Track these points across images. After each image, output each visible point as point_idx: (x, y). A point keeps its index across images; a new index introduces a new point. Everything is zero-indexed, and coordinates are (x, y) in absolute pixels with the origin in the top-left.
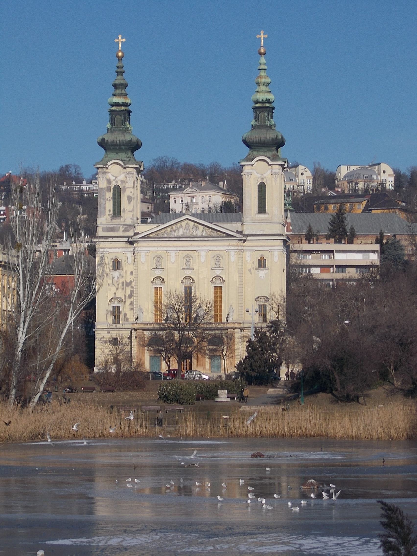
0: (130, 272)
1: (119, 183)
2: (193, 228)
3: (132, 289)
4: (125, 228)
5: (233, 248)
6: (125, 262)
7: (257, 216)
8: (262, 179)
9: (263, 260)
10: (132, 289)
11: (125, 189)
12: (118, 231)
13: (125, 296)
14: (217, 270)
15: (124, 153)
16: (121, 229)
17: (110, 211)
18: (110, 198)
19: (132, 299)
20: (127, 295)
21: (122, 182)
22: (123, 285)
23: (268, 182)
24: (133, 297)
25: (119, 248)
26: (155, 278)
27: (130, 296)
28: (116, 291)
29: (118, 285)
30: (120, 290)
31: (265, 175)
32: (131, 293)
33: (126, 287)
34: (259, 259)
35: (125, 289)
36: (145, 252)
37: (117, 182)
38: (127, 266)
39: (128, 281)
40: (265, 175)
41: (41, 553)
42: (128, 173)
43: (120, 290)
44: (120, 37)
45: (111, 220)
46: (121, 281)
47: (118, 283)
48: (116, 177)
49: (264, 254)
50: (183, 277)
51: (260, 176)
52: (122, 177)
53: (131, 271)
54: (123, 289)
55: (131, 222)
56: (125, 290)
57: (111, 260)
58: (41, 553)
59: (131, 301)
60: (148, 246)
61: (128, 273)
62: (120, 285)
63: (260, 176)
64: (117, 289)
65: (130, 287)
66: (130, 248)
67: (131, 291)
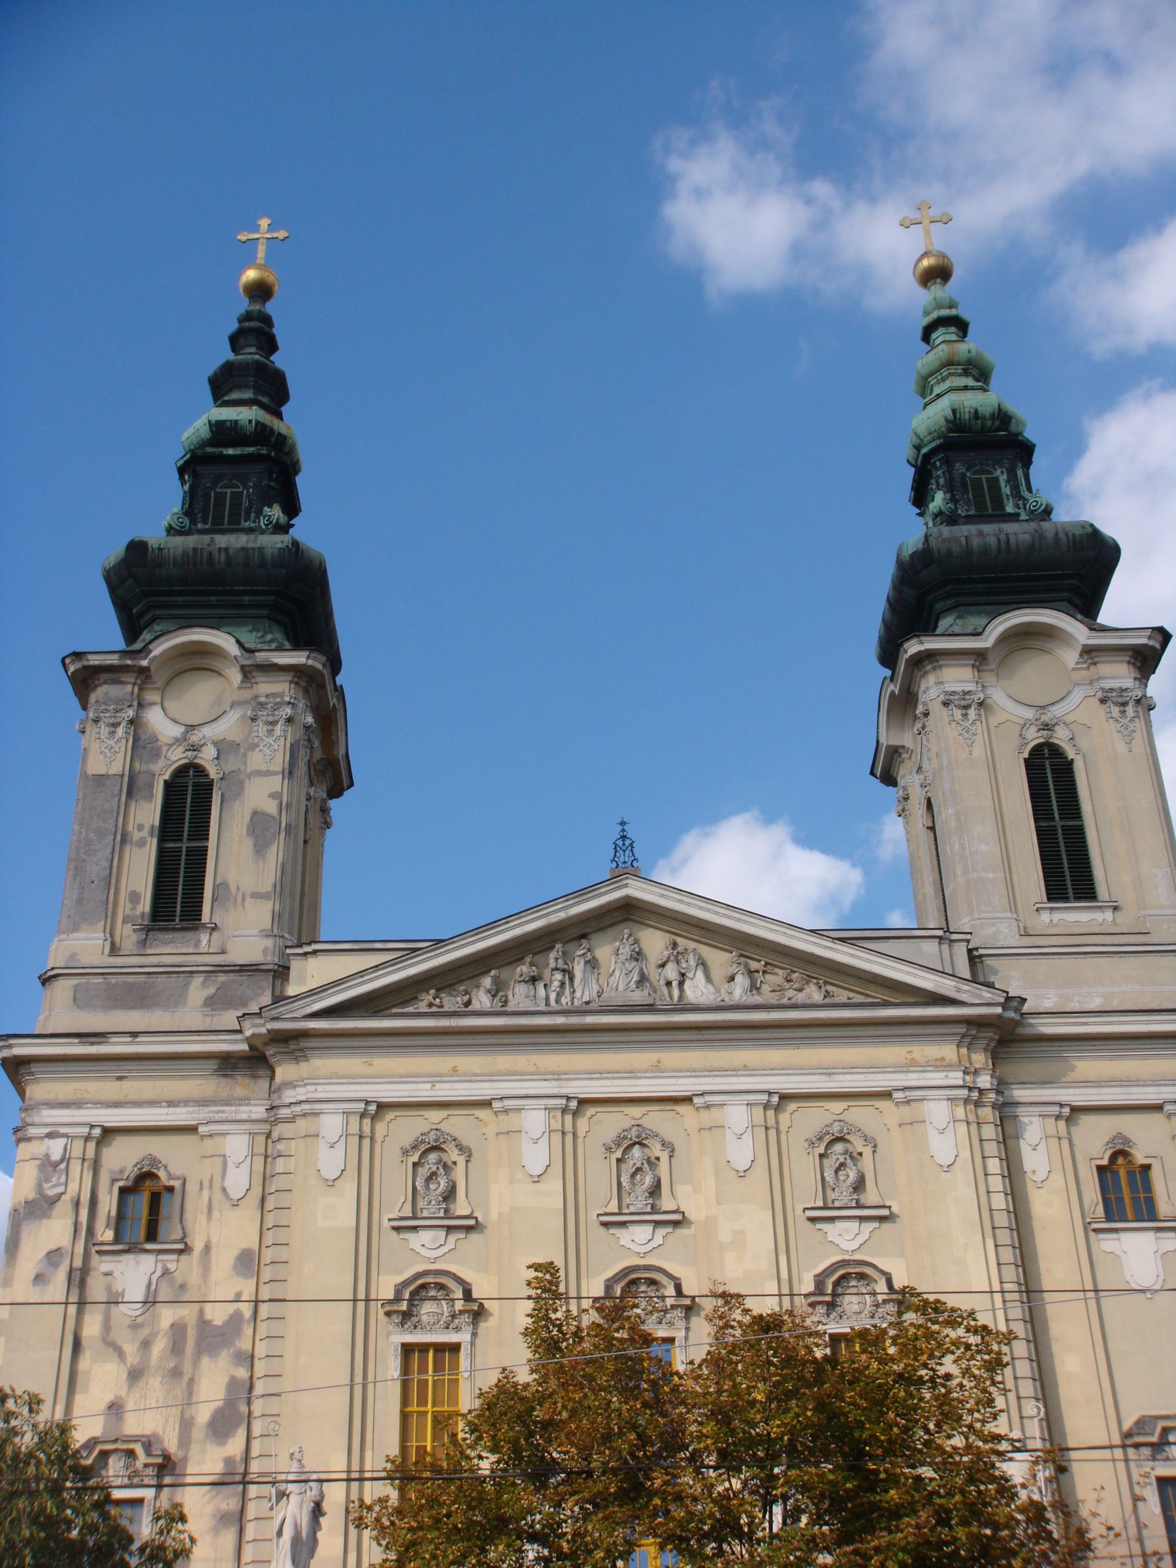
0: (236, 1253)
1: (207, 757)
2: (663, 966)
3: (242, 1373)
4: (222, 986)
5: (937, 1078)
6: (206, 1193)
7: (1045, 917)
8: (1047, 727)
9: (1131, 1174)
10: (242, 1373)
11: (236, 782)
12: (176, 1000)
13: (186, 1425)
14: (840, 1225)
15: (250, 628)
16: (198, 991)
17: (135, 897)
18: (145, 833)
19: (235, 1446)
20: (203, 1414)
21: (223, 748)
22: (177, 1348)
23: (1083, 743)
24: (241, 1433)
25: (171, 1104)
26: (406, 1284)
27: (221, 1426)
28: (123, 1393)
29: (146, 1344)
30: (155, 1387)
31: (1058, 711)
32: (230, 1403)
33: (199, 1352)
34: (1105, 1162)
35: (187, 1368)
36: (346, 1113)
37: (195, 748)
38: (216, 1214)
39: (218, 1315)
40: (1058, 711)
41: (161, 1565)
42: (262, 699)
43: (155, 1387)
44: (264, 223)
45: (143, 943)
46: (167, 1316)
47: (145, 1332)
48: (192, 727)
49: (1128, 1133)
50: (610, 1273)
51: (1029, 714)
52: (228, 726)
53: (245, 1245)
54: (176, 1373)
55: (265, 952)
56: (191, 1381)
57: (114, 1181)
58: (161, 1565)
59: (229, 1461)
60: (258, 1338)
61: (223, 1260)
62: (159, 1346)
63: (1029, 714)
64: (135, 1375)
65: (224, 1357)
66: (244, 1101)
67: (233, 1383)
